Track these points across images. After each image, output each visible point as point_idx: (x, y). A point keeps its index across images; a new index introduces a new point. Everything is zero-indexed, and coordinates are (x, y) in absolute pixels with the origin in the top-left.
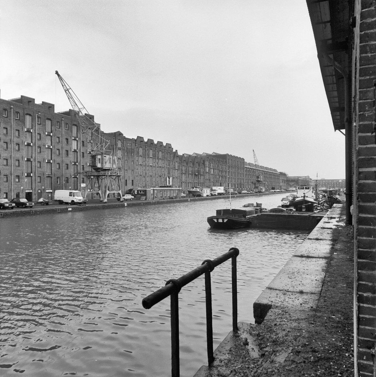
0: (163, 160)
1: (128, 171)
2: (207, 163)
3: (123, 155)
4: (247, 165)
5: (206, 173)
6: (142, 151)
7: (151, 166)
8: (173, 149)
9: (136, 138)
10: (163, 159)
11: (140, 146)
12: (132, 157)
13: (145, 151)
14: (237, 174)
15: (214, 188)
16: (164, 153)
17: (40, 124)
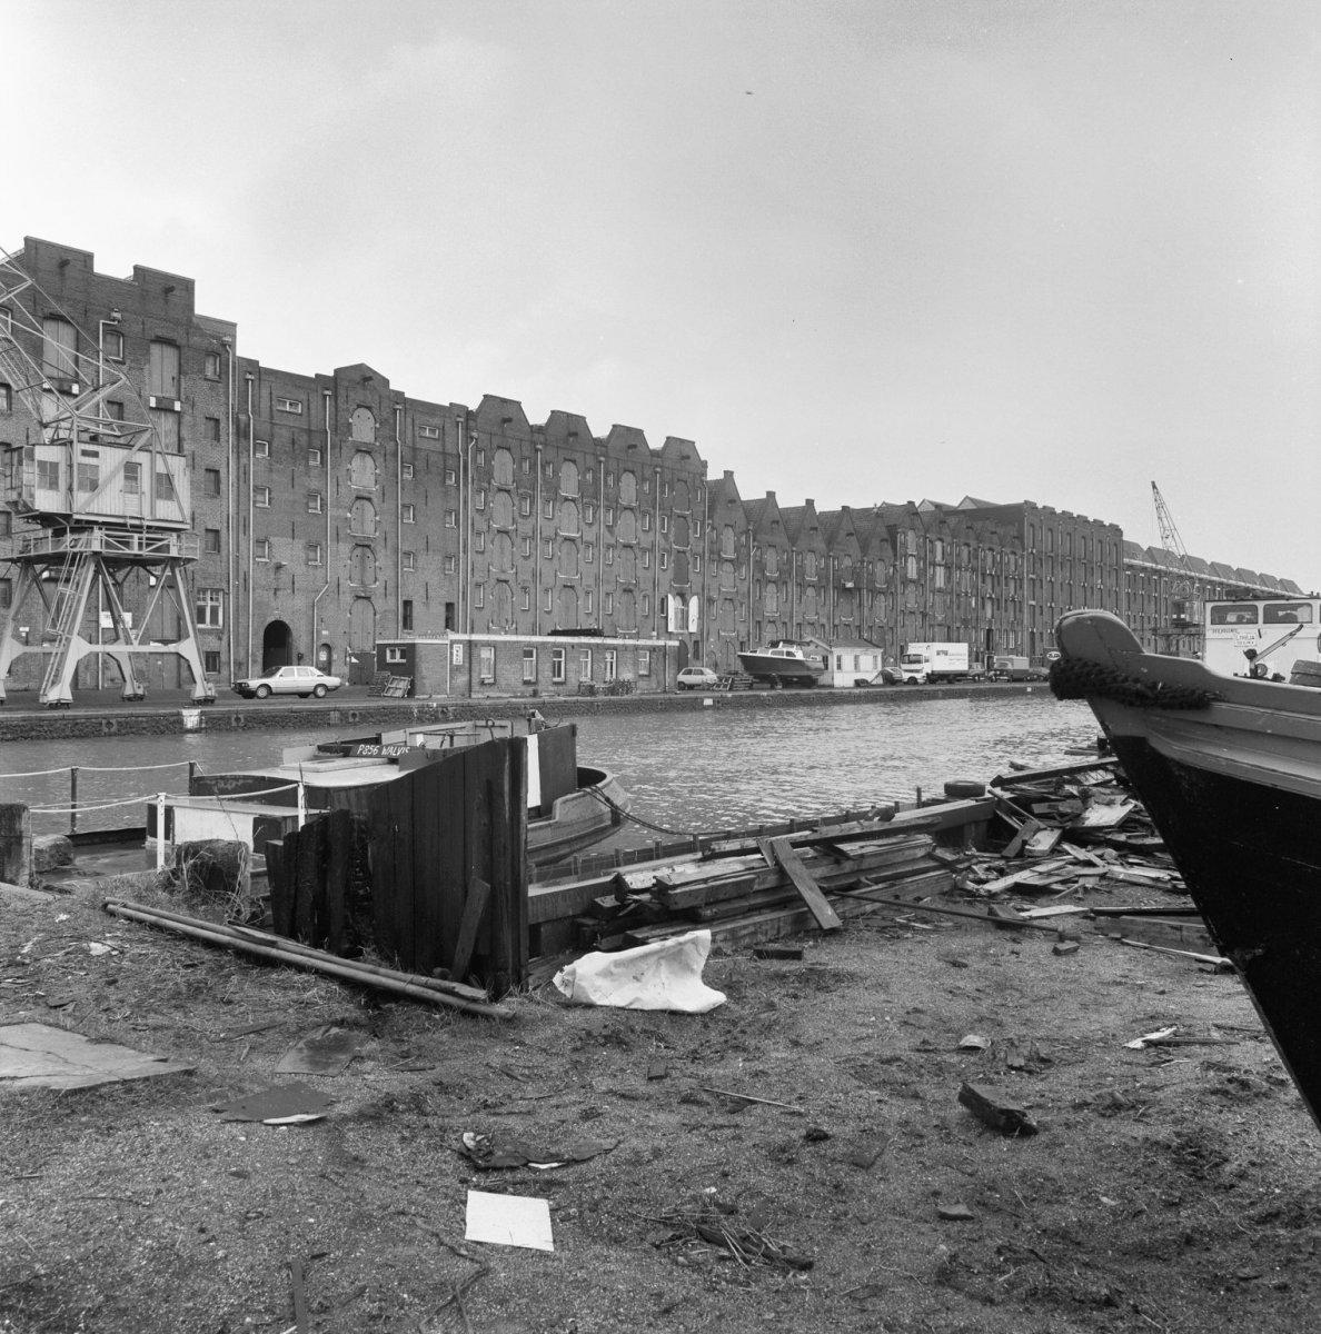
0: (644, 514)
1: (422, 560)
2: (910, 540)
3: (389, 483)
5: (906, 582)
6: (915, 566)
7: (567, 539)
8: (704, 464)
9: (473, 405)
12: (446, 494)
13: (533, 467)
15: (914, 649)
16: (653, 482)
17: (123, 363)
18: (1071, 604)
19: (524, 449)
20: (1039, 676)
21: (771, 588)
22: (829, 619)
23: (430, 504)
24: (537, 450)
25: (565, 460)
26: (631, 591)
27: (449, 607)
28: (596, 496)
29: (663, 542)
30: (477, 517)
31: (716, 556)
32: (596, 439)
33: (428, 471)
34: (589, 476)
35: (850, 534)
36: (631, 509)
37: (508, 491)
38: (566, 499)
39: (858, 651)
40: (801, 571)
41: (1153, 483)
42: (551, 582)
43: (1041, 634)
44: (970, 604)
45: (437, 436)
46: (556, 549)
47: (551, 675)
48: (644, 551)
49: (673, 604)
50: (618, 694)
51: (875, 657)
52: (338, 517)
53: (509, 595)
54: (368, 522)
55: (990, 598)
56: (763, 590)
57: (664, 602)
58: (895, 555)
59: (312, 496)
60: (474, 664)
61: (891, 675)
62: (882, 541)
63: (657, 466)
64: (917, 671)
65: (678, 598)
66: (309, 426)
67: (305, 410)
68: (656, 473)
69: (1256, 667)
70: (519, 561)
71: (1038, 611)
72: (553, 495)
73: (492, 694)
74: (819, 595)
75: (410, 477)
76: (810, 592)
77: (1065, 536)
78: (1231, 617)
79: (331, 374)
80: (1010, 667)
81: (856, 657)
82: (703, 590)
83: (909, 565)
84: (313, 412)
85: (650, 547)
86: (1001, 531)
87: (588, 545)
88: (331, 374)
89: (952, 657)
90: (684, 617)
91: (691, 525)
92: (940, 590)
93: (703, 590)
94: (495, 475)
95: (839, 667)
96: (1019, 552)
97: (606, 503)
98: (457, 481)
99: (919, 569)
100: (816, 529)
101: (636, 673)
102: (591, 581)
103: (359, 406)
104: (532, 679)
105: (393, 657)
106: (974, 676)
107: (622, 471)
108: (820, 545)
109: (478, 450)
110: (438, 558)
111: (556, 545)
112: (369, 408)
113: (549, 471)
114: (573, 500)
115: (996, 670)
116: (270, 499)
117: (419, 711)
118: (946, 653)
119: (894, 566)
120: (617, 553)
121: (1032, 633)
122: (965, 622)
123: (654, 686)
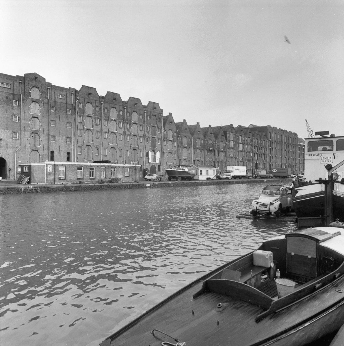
0: (141, 125)
1: (58, 138)
2: (231, 136)
4: (301, 142)
5: (230, 148)
6: (233, 144)
7: (112, 133)
10: (140, 124)
11: (86, 100)
13: (100, 109)
14: (284, 153)
15: (229, 168)
18: (286, 156)
19: (97, 103)
20: (269, 177)
21: (185, 149)
22: (204, 159)
23: (61, 120)
24: (101, 104)
25: (112, 107)
26: (136, 150)
27: (68, 154)
28: (123, 119)
29: (147, 134)
30: (79, 125)
31: (166, 139)
32: (123, 101)
33: (60, 109)
34: (121, 113)
35: (211, 133)
36: (136, 124)
37: (91, 117)
38: (112, 120)
39: (208, 169)
40: (195, 144)
41: (306, 120)
42: (107, 146)
43: (273, 164)
44: (250, 155)
45: (64, 98)
46: (109, 136)
47: (89, 176)
48: (140, 137)
49: (150, 154)
50: (113, 183)
51: (214, 171)
52: (25, 124)
53: (91, 150)
54: (37, 125)
55: (257, 153)
56: (182, 150)
57: (147, 154)
58: (226, 140)
59: (15, 116)
60: (57, 172)
61: (219, 176)
62: (222, 136)
63: (145, 110)
64: (229, 175)
65: (153, 152)
66: (14, 92)
67: (12, 87)
68: (145, 112)
69: (332, 175)
70: (95, 139)
71: (272, 157)
72: (107, 118)
73: (64, 183)
74: (201, 151)
75: (53, 111)
76: (198, 151)
77: (280, 136)
78: (320, 148)
79: (23, 76)
80: (260, 174)
81: (207, 171)
82: (161, 150)
83: (231, 143)
84: (15, 88)
85: (143, 136)
86: (260, 134)
87: (120, 134)
88: (23, 76)
89: (241, 171)
90: (154, 159)
91: (157, 129)
92: (241, 151)
93: (161, 150)
94: (86, 111)
95: (201, 174)
96: (266, 140)
97: (127, 121)
98: (72, 113)
99: (234, 145)
100: (200, 131)
101: (124, 175)
102: (121, 146)
103: (33, 87)
104: (81, 177)
105: (26, 170)
106: (248, 177)
107: (132, 111)
108: (201, 136)
109: (80, 103)
110: (64, 138)
111: (109, 134)
112: (38, 88)
113: (106, 111)
114: (115, 120)
115: (256, 175)
116: (18, 119)
117: (24, 189)
118: (239, 170)
119: (226, 143)
120: (131, 137)
121: (270, 164)
122: (249, 160)
123: (131, 180)
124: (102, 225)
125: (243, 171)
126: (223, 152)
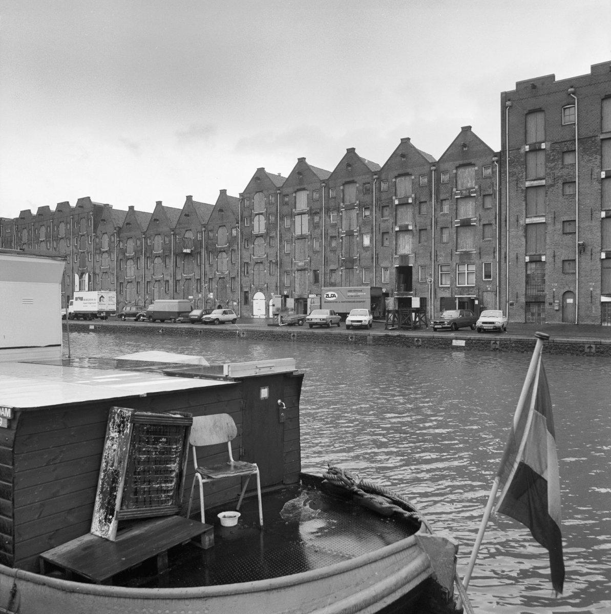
31: (99, 251)
92: (302, 237)
124: (472, 429)
125: (92, 302)
126: (227, 254)
